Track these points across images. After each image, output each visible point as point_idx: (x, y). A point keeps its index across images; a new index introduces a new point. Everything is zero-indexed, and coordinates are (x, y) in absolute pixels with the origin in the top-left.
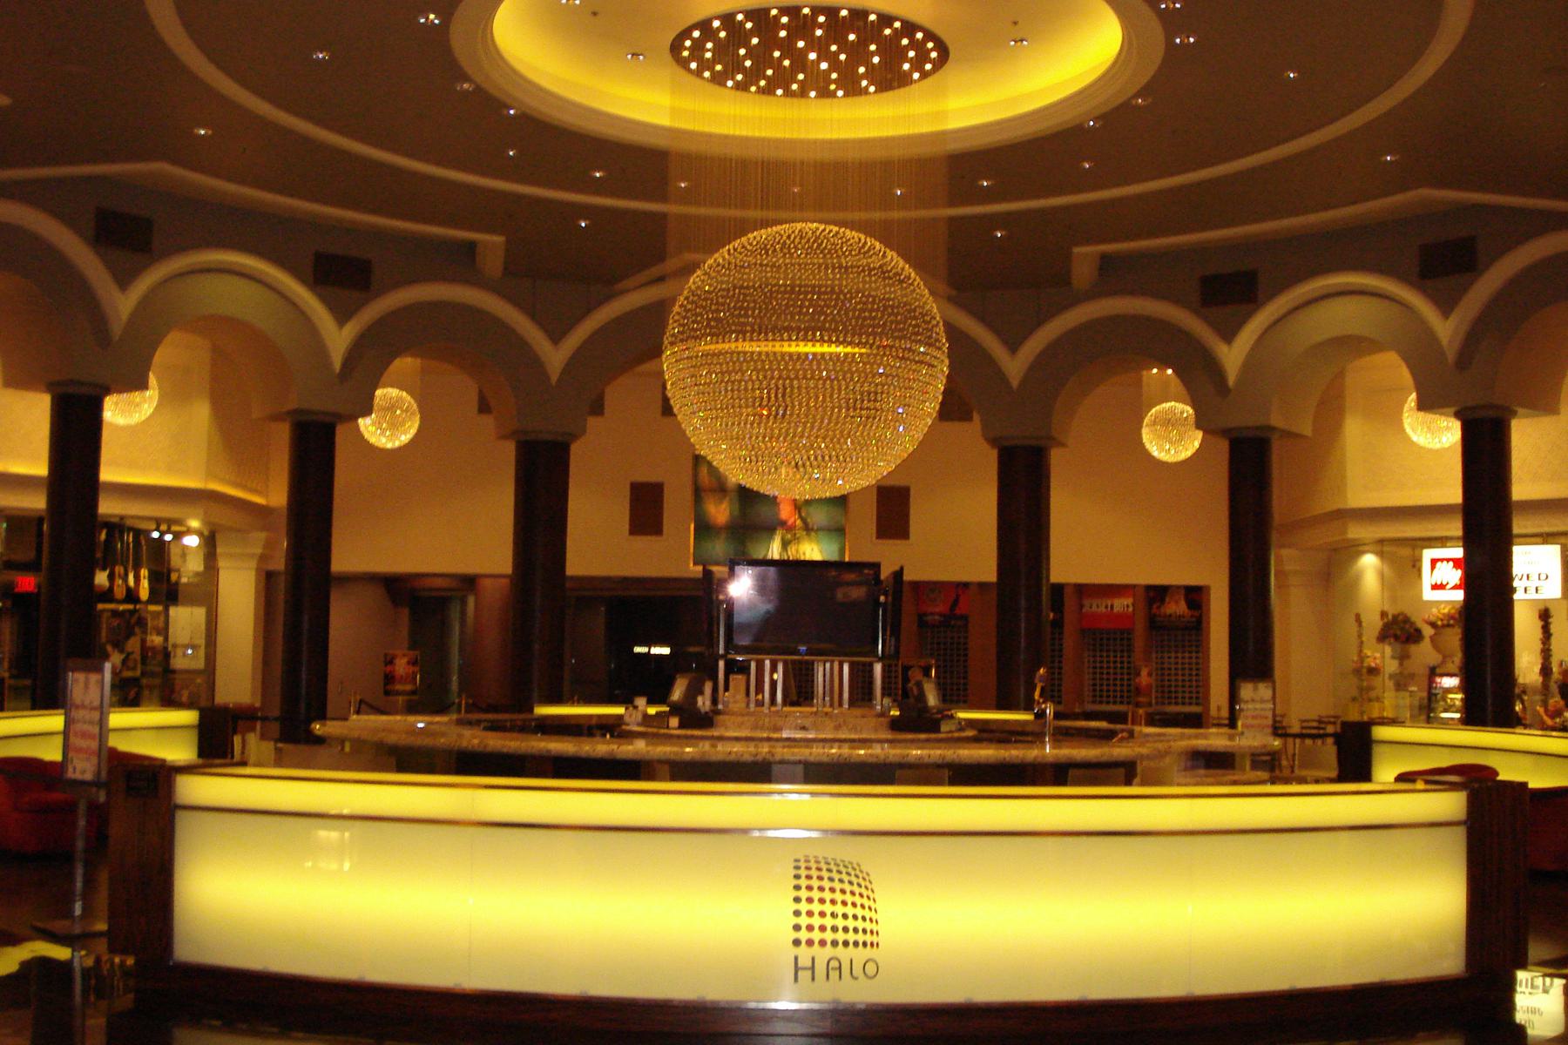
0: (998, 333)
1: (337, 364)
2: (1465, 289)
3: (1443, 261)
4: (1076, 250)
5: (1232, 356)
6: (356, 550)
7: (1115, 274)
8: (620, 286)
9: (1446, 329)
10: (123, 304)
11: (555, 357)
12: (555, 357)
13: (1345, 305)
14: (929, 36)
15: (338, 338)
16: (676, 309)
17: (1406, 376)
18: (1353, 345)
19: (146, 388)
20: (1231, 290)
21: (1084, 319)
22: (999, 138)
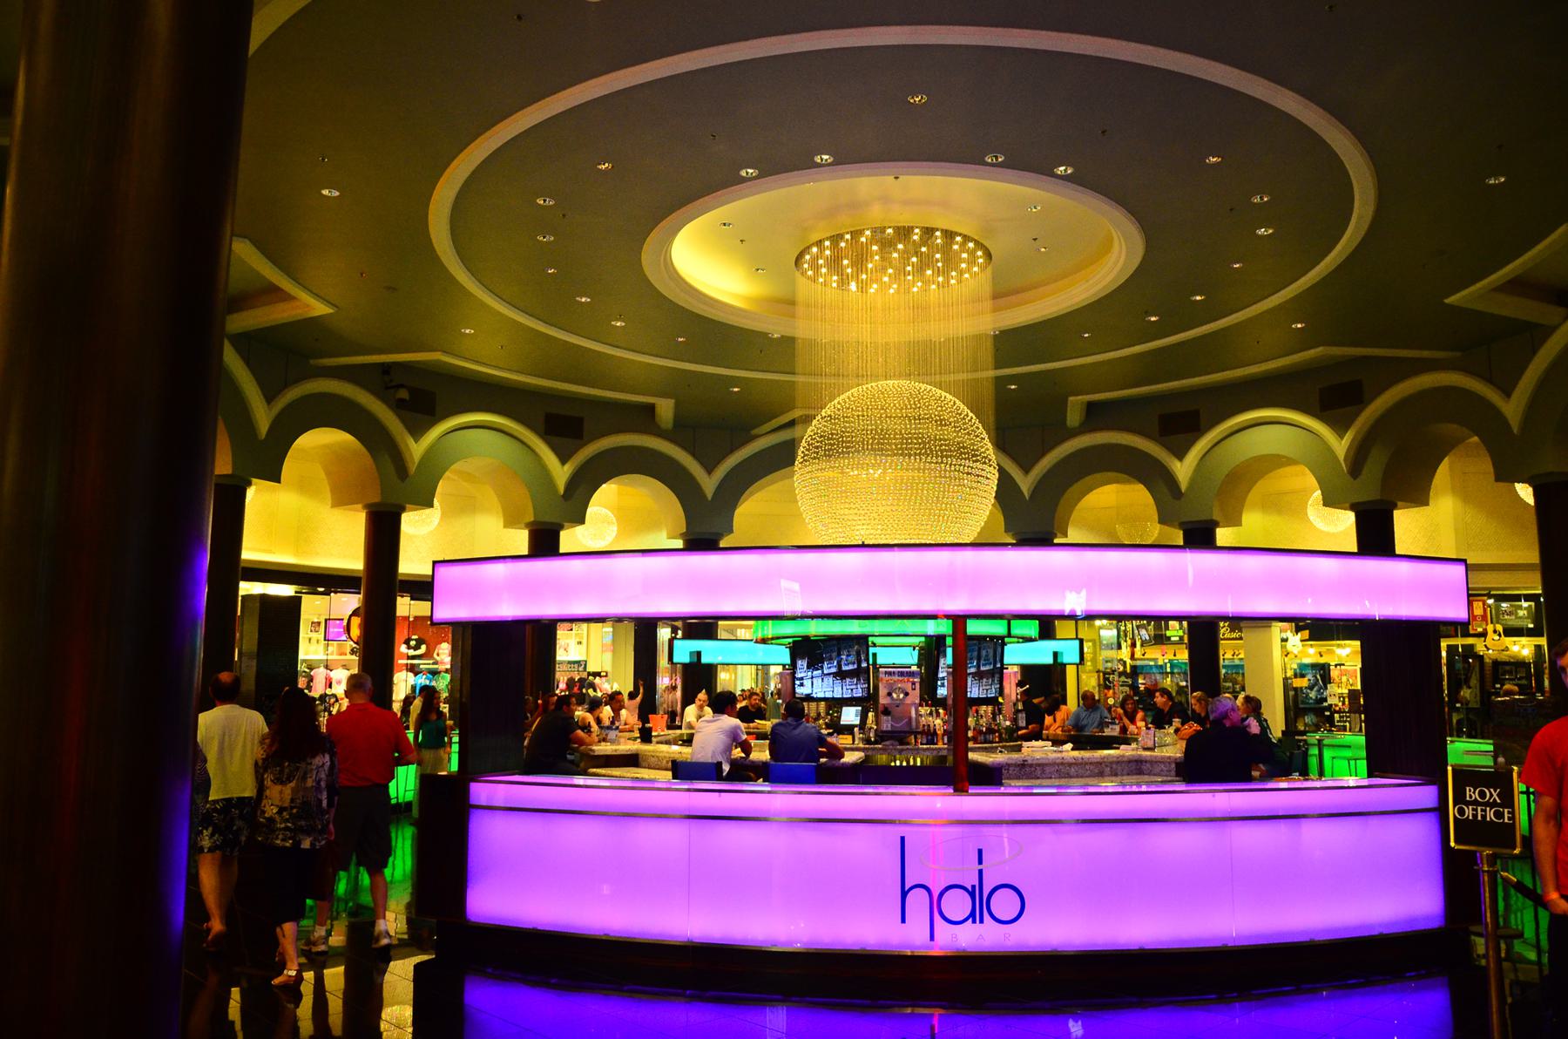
0: (1490, 380)
1: (561, 490)
2: (1357, 414)
3: (1331, 396)
4: (1071, 398)
5: (1183, 470)
6: (1365, 782)
7: (1097, 415)
8: (755, 432)
9: (1341, 446)
10: (416, 449)
11: (709, 484)
12: (709, 484)
13: (1277, 434)
14: (979, 245)
15: (561, 473)
16: (804, 443)
17: (1312, 481)
18: (1275, 462)
19: (431, 506)
20: (1181, 422)
21: (1544, 366)
22: (1069, 303)
